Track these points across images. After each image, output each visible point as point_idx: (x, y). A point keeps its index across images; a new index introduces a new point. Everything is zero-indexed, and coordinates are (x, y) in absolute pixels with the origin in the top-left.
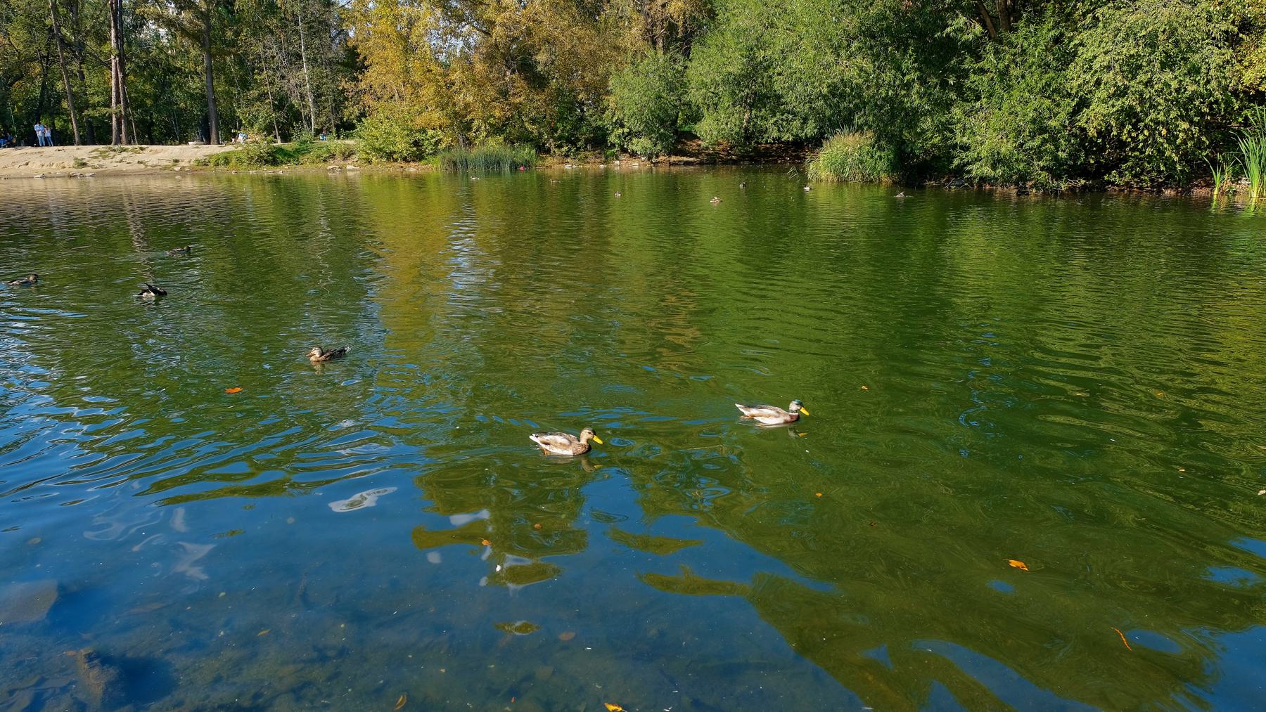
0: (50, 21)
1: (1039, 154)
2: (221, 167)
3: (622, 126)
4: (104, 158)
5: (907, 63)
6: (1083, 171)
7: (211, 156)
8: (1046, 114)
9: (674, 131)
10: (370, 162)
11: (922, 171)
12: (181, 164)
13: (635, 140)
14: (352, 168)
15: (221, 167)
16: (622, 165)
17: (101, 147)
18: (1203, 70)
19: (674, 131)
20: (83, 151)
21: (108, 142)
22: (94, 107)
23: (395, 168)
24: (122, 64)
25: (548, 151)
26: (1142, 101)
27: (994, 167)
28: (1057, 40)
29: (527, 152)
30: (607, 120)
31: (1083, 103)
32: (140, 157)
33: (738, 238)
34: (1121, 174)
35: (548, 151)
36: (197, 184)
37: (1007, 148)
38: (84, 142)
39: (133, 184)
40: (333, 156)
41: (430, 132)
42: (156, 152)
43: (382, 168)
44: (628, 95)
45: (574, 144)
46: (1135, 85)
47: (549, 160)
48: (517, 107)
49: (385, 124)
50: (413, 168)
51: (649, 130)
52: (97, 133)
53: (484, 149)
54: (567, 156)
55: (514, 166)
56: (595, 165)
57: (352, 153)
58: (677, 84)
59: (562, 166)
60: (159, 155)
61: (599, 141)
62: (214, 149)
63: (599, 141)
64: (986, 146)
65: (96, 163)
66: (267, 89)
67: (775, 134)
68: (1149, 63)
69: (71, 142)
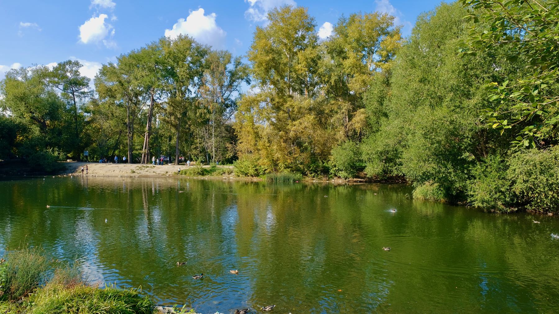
1: (499, 199)
2: (183, 175)
3: (335, 166)
4: (141, 169)
5: (449, 166)
6: (517, 205)
8: (500, 186)
9: (356, 169)
10: (239, 176)
11: (455, 198)
12: (169, 173)
13: (340, 172)
15: (183, 175)
16: (335, 181)
17: (139, 165)
18: (555, 175)
19: (356, 169)
20: (134, 166)
21: (139, 163)
23: (249, 179)
24: (149, 136)
25: (307, 175)
26: (534, 185)
27: (483, 204)
28: (503, 161)
29: (299, 175)
30: (330, 164)
31: (514, 182)
32: (154, 170)
34: (531, 206)
35: (307, 175)
37: (487, 198)
40: (224, 173)
41: (262, 167)
42: (159, 168)
43: (243, 179)
44: (338, 157)
45: (316, 172)
46: (531, 179)
47: (307, 179)
48: (295, 158)
49: (245, 162)
50: (255, 179)
51: (346, 170)
52: (135, 160)
54: (314, 177)
55: (294, 181)
56: (324, 181)
57: (232, 172)
58: (357, 153)
59: (312, 181)
60: (161, 169)
61: (326, 171)
63: (326, 171)
64: (479, 195)
65: (138, 171)
66: (198, 145)
67: (396, 173)
68: (535, 172)
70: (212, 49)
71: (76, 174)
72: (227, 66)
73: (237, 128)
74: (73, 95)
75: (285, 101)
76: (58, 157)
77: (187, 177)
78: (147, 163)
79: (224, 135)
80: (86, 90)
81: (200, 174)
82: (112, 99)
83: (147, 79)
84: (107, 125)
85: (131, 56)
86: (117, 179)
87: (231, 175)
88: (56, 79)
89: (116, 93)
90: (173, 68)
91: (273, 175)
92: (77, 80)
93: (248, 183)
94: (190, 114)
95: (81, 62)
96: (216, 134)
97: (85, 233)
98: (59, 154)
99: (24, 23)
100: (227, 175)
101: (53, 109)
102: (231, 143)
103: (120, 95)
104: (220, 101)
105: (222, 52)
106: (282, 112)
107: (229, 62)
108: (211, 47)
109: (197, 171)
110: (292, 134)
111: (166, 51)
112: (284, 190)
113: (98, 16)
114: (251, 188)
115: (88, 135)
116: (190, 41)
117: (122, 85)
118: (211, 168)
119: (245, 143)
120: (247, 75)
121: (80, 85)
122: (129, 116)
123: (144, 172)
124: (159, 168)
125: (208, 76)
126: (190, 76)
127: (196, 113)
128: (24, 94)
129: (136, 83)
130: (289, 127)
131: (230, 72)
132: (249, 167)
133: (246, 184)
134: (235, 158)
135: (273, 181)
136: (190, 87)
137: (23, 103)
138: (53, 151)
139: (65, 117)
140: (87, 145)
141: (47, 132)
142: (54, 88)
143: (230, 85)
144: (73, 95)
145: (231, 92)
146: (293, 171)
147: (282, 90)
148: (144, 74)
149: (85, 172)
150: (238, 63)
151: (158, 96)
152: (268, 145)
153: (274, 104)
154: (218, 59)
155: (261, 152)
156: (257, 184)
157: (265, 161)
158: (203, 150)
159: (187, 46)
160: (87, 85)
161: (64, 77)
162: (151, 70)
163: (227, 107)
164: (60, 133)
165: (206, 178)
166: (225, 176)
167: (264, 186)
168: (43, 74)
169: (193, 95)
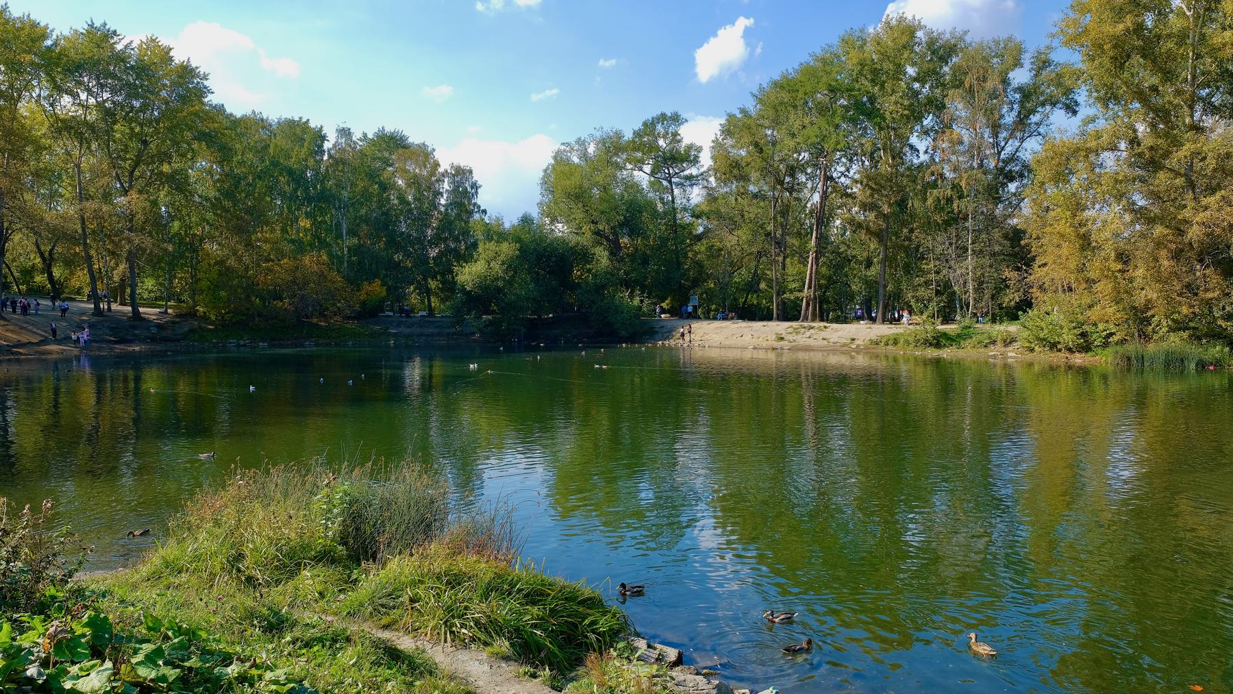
0: (770, 228)
2: (890, 347)
4: (797, 333)
7: (882, 337)
10: (1032, 350)
12: (857, 342)
14: (1012, 353)
17: (794, 324)
22: (791, 292)
23: (1059, 358)
24: (817, 259)
33: (953, 42)
36: (867, 359)
38: (779, 319)
39: (817, 357)
40: (994, 342)
41: (1101, 326)
42: (837, 331)
43: (1044, 357)
48: (1209, 303)
49: (1053, 314)
50: (1078, 359)
52: (790, 313)
53: (1165, 345)
55: (1202, 365)
57: (1013, 340)
60: (839, 334)
62: (882, 330)
65: (791, 338)
66: (932, 276)
69: (768, 318)
70: (968, 38)
71: (672, 343)
72: (1011, 75)
73: (1033, 230)
74: (670, 182)
75: (1178, 144)
76: (640, 308)
77: (899, 351)
78: (813, 320)
79: (997, 248)
80: (694, 171)
81: (931, 345)
82: (742, 183)
83: (811, 132)
84: (734, 240)
85: (782, 87)
86: (747, 355)
87: (1011, 348)
88: (639, 154)
89: (747, 170)
90: (872, 100)
91: (1131, 348)
92: (678, 152)
93: (1058, 367)
94: (915, 204)
95: (684, 115)
96: (978, 247)
97: (695, 463)
98: (642, 301)
99: (606, 60)
100: (999, 348)
101: (632, 215)
102: (1018, 269)
103: (758, 174)
104: (992, 164)
105: (997, 43)
106: (1162, 175)
107: (1017, 63)
108: (966, 33)
109: (924, 336)
110: (1194, 233)
111: (855, 61)
112: (1163, 390)
113: (733, 23)
114: (1067, 383)
115: (699, 265)
116: (909, 27)
117: (761, 151)
118: (959, 331)
119: (1054, 264)
120: (1068, 91)
121: (682, 161)
122: (775, 218)
123: (802, 339)
124: (837, 331)
125: (957, 106)
126: (913, 112)
127: (925, 200)
128: (581, 187)
129: (792, 144)
130: (1186, 214)
131: (1020, 89)
132: (1062, 328)
133: (1053, 368)
134: (1026, 304)
135: (1131, 365)
136: (914, 140)
137: (580, 205)
138: (631, 296)
139: (656, 230)
140: (696, 283)
141: (622, 260)
142: (636, 173)
143: (1022, 122)
144: (670, 182)
145: (1022, 140)
146: (1199, 338)
147: (1167, 113)
148: (807, 121)
149: (687, 337)
150: (1042, 64)
151: (843, 169)
152: (1119, 267)
153: (1140, 155)
154: (986, 60)
155: (1099, 287)
156: (1084, 373)
157: (1110, 311)
158: (944, 289)
159: (904, 39)
160: (695, 161)
161: (652, 148)
162: (823, 110)
163: (1012, 179)
164: (645, 261)
165: (946, 353)
166: (993, 351)
167: (1104, 377)
168: (613, 147)
169: (924, 158)
